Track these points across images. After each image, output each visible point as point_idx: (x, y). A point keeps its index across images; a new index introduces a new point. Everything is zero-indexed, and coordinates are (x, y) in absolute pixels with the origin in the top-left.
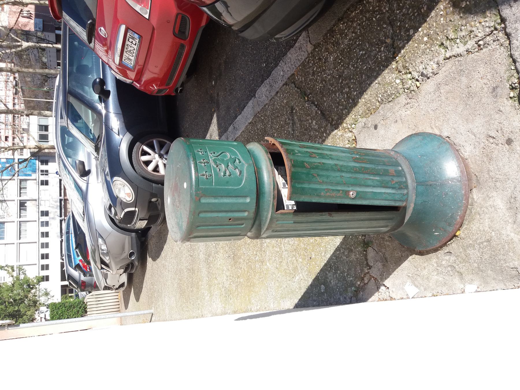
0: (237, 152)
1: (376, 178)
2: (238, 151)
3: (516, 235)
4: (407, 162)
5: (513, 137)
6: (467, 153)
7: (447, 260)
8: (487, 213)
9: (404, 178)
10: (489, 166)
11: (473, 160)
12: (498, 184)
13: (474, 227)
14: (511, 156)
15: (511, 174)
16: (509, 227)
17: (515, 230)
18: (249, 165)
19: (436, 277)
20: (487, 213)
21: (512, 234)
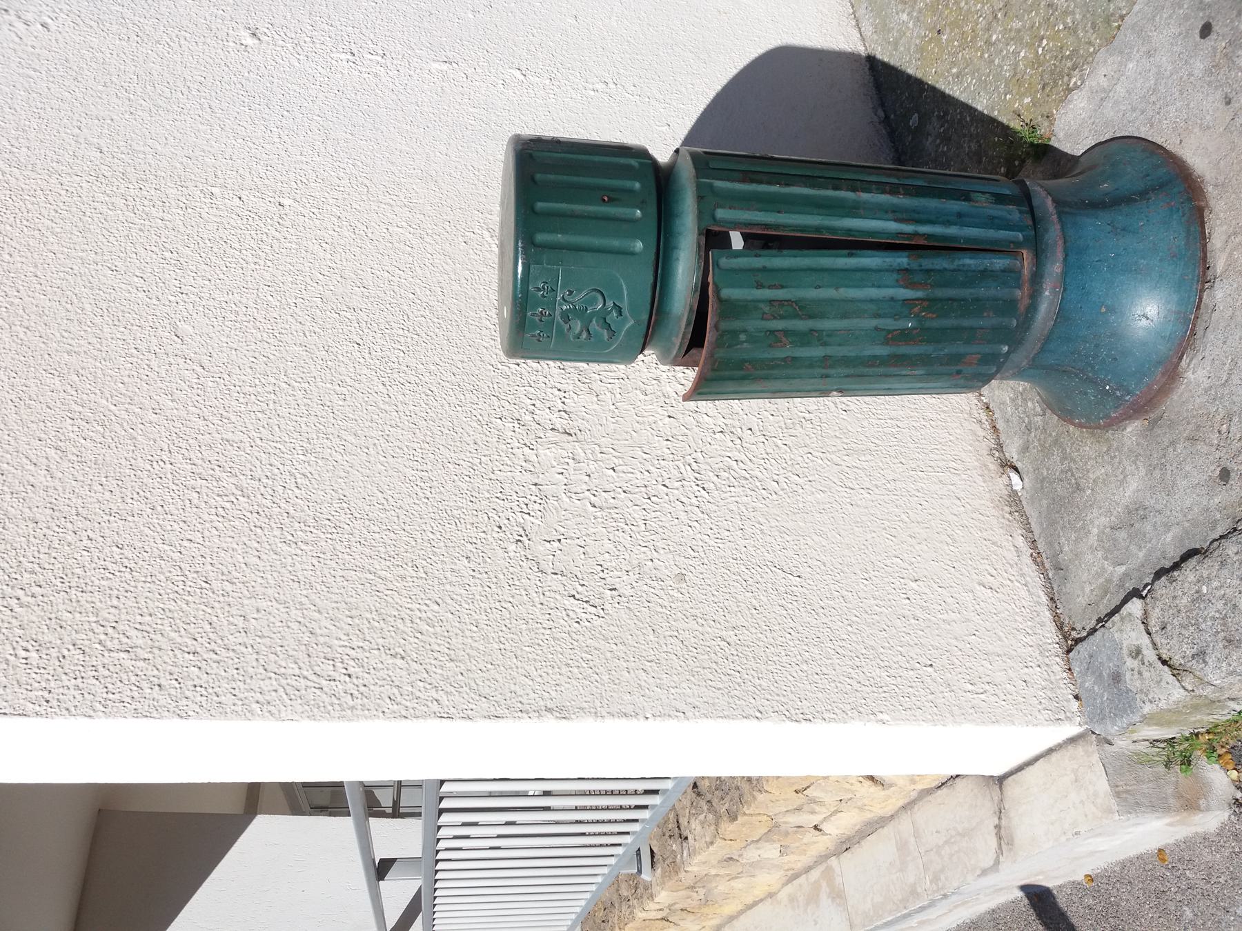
0: (624, 287)
1: (916, 372)
2: (627, 289)
3: (1096, 538)
4: (1052, 323)
5: (1232, 482)
6: (1192, 377)
7: (1034, 409)
8: (1113, 465)
9: (995, 369)
10: (1182, 441)
11: (1186, 395)
12: (1157, 473)
13: (1088, 448)
14: (1203, 488)
15: (1177, 497)
16: (1104, 520)
17: (1104, 533)
18: (638, 322)
19: (1008, 398)
20: (1113, 465)
21: (1095, 531)
